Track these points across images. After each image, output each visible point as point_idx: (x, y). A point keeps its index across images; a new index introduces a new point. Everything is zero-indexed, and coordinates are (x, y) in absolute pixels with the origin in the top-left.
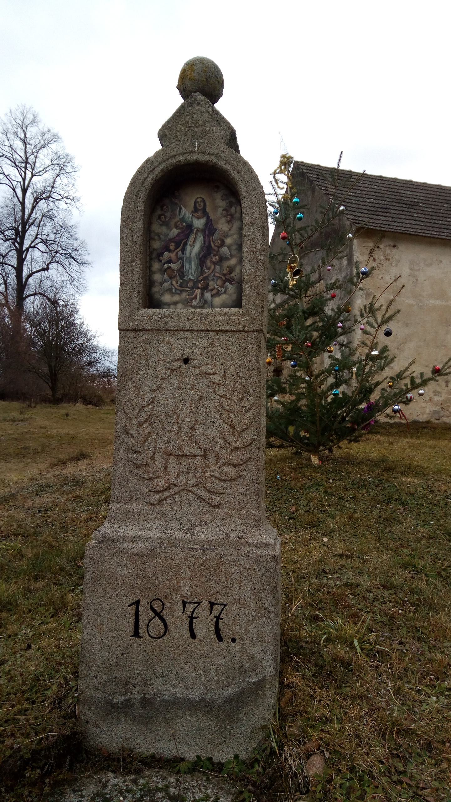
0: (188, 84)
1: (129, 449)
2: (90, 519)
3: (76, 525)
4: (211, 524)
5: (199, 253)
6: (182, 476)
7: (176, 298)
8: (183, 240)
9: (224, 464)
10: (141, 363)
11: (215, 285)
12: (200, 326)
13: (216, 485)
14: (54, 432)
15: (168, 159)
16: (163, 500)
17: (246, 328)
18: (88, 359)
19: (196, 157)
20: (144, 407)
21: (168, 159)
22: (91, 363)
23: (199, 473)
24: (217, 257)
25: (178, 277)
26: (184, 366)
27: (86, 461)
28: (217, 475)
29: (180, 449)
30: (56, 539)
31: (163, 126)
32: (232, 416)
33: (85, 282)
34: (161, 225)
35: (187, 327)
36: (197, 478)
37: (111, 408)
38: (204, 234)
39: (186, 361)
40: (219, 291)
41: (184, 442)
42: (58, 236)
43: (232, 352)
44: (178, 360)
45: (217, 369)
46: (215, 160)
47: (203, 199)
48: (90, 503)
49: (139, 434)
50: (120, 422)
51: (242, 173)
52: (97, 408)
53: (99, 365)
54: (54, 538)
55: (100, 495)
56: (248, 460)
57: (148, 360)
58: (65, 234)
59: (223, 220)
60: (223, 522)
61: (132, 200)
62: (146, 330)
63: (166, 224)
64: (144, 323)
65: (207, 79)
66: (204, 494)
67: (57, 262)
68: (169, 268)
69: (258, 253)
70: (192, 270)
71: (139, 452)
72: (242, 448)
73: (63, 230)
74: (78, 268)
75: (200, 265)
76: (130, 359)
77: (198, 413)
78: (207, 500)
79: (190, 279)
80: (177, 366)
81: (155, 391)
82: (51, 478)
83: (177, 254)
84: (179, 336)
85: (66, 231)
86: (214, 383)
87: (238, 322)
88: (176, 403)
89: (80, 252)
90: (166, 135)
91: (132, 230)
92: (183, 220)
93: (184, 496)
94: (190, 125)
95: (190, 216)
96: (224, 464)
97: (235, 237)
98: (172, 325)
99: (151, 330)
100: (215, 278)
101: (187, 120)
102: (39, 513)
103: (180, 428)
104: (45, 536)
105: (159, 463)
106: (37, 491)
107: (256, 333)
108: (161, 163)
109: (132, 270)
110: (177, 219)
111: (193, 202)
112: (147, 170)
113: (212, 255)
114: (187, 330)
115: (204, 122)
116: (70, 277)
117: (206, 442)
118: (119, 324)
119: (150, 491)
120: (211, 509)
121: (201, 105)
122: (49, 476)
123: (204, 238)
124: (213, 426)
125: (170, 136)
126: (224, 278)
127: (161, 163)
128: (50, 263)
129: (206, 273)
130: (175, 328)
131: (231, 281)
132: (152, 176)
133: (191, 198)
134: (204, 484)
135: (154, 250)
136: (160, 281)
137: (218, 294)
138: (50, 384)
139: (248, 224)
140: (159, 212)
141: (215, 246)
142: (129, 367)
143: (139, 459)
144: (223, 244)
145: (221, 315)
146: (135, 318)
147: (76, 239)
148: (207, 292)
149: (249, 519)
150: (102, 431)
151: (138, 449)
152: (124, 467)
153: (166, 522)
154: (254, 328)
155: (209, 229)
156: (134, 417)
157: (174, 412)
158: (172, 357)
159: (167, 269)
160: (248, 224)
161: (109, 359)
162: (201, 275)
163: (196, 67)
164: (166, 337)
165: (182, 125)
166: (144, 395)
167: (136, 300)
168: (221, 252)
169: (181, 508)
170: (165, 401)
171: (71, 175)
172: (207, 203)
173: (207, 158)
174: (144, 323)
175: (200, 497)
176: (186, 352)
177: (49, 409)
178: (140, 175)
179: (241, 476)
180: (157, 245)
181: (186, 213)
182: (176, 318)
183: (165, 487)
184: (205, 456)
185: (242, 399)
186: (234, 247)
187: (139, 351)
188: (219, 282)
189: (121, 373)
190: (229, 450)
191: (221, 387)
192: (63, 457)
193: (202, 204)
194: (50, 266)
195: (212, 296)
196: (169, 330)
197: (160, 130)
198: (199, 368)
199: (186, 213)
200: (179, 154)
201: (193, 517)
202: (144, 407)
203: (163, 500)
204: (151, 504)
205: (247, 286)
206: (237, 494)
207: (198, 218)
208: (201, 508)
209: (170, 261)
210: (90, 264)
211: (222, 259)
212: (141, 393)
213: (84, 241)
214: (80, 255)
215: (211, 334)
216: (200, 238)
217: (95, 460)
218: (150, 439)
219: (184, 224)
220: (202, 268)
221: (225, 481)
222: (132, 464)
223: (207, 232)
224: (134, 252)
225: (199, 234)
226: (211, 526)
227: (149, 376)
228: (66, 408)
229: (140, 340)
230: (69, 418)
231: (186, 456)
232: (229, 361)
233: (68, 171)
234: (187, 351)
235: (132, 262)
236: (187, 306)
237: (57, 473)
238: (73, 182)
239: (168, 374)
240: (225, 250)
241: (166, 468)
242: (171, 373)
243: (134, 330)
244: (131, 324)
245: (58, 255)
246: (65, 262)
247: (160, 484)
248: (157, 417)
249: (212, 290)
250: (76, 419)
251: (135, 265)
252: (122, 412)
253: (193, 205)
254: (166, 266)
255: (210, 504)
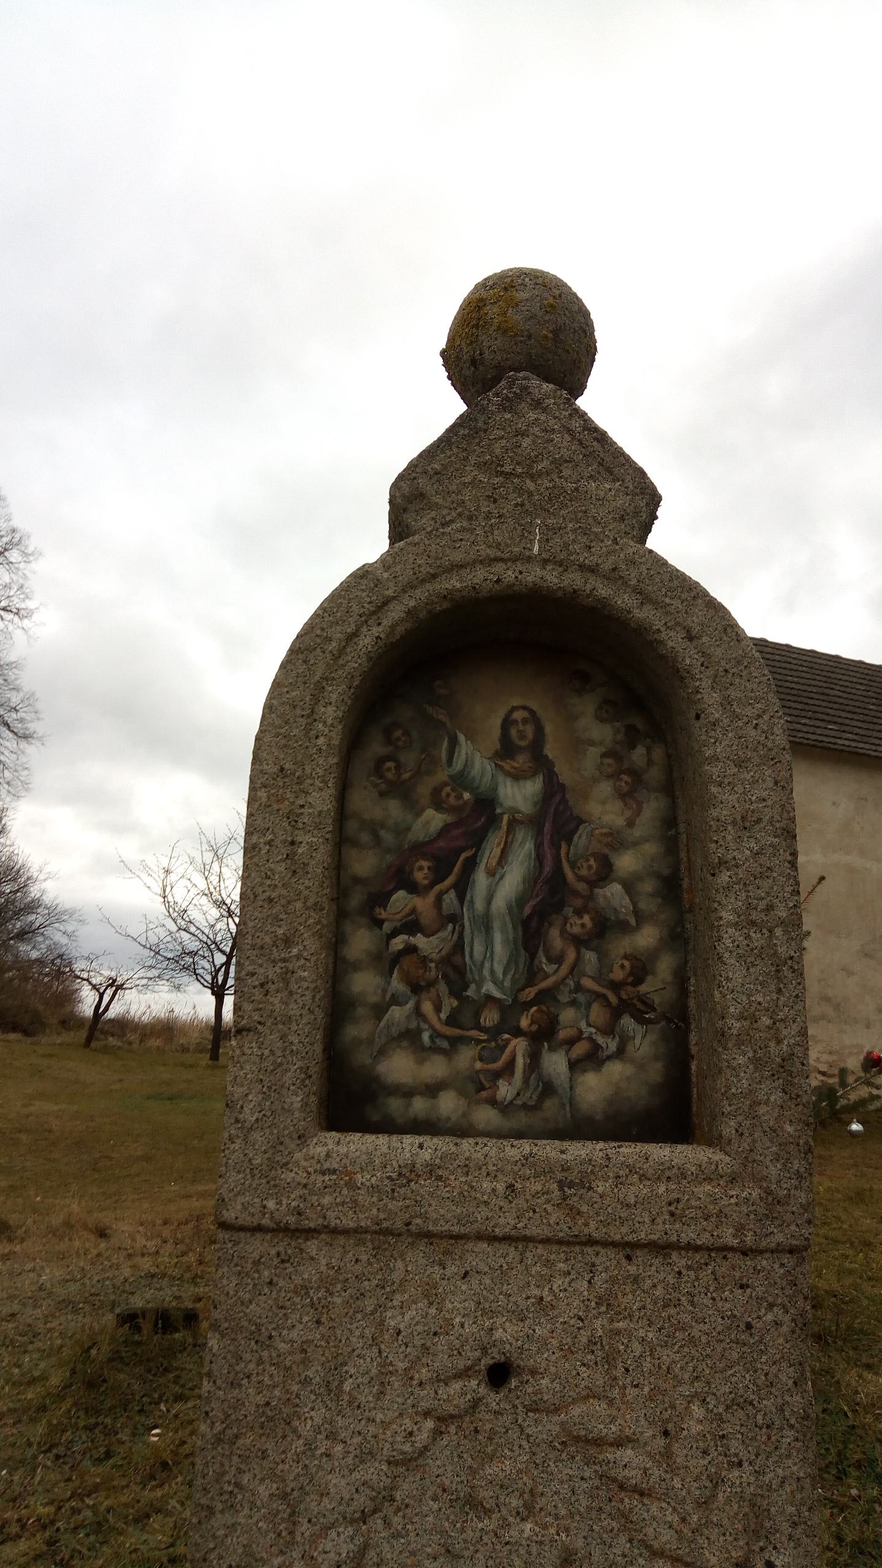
0: (492, 345)
5: (522, 900)
7: (436, 1068)
8: (463, 850)
10: (307, 1381)
11: (583, 1024)
15: (434, 576)
19: (533, 575)
21: (434, 576)
24: (586, 919)
25: (443, 988)
26: (493, 1399)
31: (412, 466)
33: (25, 773)
34: (382, 794)
35: (506, 1223)
38: (539, 832)
40: (597, 1047)
44: (464, 1374)
45: (635, 1421)
46: (604, 591)
47: (532, 712)
51: (704, 639)
52: (29, 1040)
53: (40, 939)
57: (337, 1366)
59: (605, 788)
61: (298, 712)
62: (335, 1232)
63: (400, 790)
64: (326, 1200)
65: (555, 332)
68: (411, 949)
69: (778, 932)
70: (493, 960)
74: (15, 745)
75: (526, 949)
76: (260, 1362)
79: (489, 998)
80: (463, 1403)
83: (439, 899)
84: (472, 1262)
86: (622, 1487)
89: (20, 715)
90: (422, 495)
91: (292, 818)
92: (461, 780)
94: (507, 468)
95: (489, 767)
97: (651, 849)
98: (441, 1214)
99: (356, 1231)
100: (581, 998)
101: (498, 451)
107: (786, 1259)
108: (410, 586)
109: (286, 976)
110: (442, 776)
111: (496, 722)
112: (356, 609)
113: (568, 911)
114: (507, 1239)
115: (558, 464)
121: (544, 410)
123: (538, 846)
125: (438, 499)
126: (613, 999)
127: (410, 586)
129: (547, 976)
130: (456, 1229)
131: (640, 1010)
132: (376, 631)
133: (490, 710)
135: (357, 880)
136: (373, 999)
137: (594, 1059)
139: (734, 823)
140: (376, 748)
141: (580, 878)
144: (605, 872)
145: (643, 1177)
146: (289, 1176)
147: (17, 689)
148: (552, 1049)
154: (779, 1238)
155: (557, 818)
158: (442, 1361)
159: (401, 954)
160: (734, 823)
161: (62, 928)
162: (530, 982)
163: (522, 295)
164: (415, 1261)
165: (478, 466)
166: (314, 1540)
167: (296, 1101)
168: (601, 901)
171: (18, 569)
172: (548, 729)
173: (573, 580)
174: (326, 1200)
176: (498, 1334)
178: (331, 624)
180: (364, 864)
181: (474, 757)
182: (457, 1181)
186: (648, 886)
188: (598, 1013)
191: (654, 1509)
193: (529, 731)
195: (574, 1066)
196: (429, 1236)
197: (401, 477)
198: (556, 1410)
199: (474, 757)
200: (475, 561)
205: (741, 1060)
207: (517, 777)
209: (412, 926)
211: (605, 927)
212: (304, 1528)
213: (33, 694)
215: (606, 1258)
216: (524, 848)
219: (467, 796)
220: (532, 956)
223: (547, 827)
224: (299, 905)
225: (520, 834)
227: (339, 1448)
229: (308, 1273)
232: (680, 1383)
233: (12, 560)
234: (507, 1333)
235: (288, 942)
236: (479, 1102)
238: (21, 581)
239: (422, 1438)
240: (613, 894)
242: (437, 1433)
243: (281, 1230)
244: (271, 1204)
249: (571, 1042)
251: (298, 957)
253: (496, 733)
254: (398, 943)
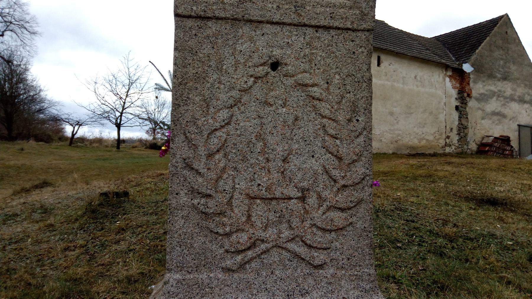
1: (194, 192)
2: (67, 249)
3: (53, 257)
4: (315, 292)
6: (272, 228)
9: (329, 209)
10: (210, 66)
12: (293, 18)
13: (319, 238)
14: (12, 163)
16: (245, 263)
17: (355, 26)
18: (38, 107)
20: (216, 130)
22: (40, 111)
23: (295, 222)
26: (273, 73)
27: (50, 189)
28: (319, 224)
29: (268, 189)
30: (33, 275)
32: (339, 143)
33: (35, 48)
35: (277, 18)
36: (293, 229)
37: (59, 144)
39: (275, 66)
41: (275, 180)
42: (11, 10)
43: (336, 57)
45: (317, 80)
48: (65, 231)
49: (209, 169)
50: (179, 153)
52: (48, 144)
54: (31, 275)
55: (74, 223)
56: (360, 202)
57: (220, 62)
58: (18, 9)
60: (330, 288)
62: (218, 18)
64: (214, 7)
66: (302, 250)
67: (11, 31)
71: (209, 196)
72: (351, 186)
73: (16, 6)
76: (193, 60)
77: (292, 139)
78: (308, 259)
80: (263, 73)
81: (231, 107)
82: (16, 206)
85: (19, 7)
86: (313, 98)
87: (344, 16)
88: (262, 124)
93: (275, 256)
96: (329, 209)
102: (9, 245)
103: (268, 160)
104: (20, 274)
105: (238, 212)
106: (4, 221)
114: (277, 23)
116: (22, 43)
117: (303, 179)
118: (176, 7)
119: (227, 251)
120: (313, 270)
122: (14, 203)
124: (313, 156)
128: (5, 31)
130: (260, 19)
134: (302, 237)
138: (6, 125)
142: (191, 71)
143: (210, 205)
145: (322, 6)
149: (362, 280)
150: (54, 162)
151: (209, 192)
152: (186, 218)
153: (252, 295)
154: (365, 26)
156: (201, 145)
157: (259, 137)
158: (256, 60)
164: (246, 30)
166: (215, 113)
169: (272, 273)
170: (247, 122)
174: (214, 7)
175: (297, 256)
176: (274, 53)
177: (5, 145)
179: (351, 223)
183: (248, 245)
184: (303, 199)
185: (350, 120)
187: (207, 49)
189: (180, 80)
190: (335, 189)
192: (28, 185)
194: (6, 33)
196: (251, 21)
201: (290, 284)
202: (216, 130)
203: (245, 263)
204: (228, 270)
206: (345, 248)
208: (299, 270)
210: (40, 34)
212: (212, 110)
214: (31, 27)
217: (58, 187)
218: (225, 176)
221: (330, 231)
222: (198, 213)
226: (315, 295)
228: (20, 144)
229: (209, 32)
230: (24, 152)
231: (276, 199)
232: (333, 69)
234: (277, 52)
237: (22, 200)
241: (249, 216)
242: (255, 82)
244: (194, 8)
245: (12, 25)
246: (18, 31)
247: (241, 241)
248: (235, 144)
250: (30, 153)
252: (183, 137)
255: (312, 265)
